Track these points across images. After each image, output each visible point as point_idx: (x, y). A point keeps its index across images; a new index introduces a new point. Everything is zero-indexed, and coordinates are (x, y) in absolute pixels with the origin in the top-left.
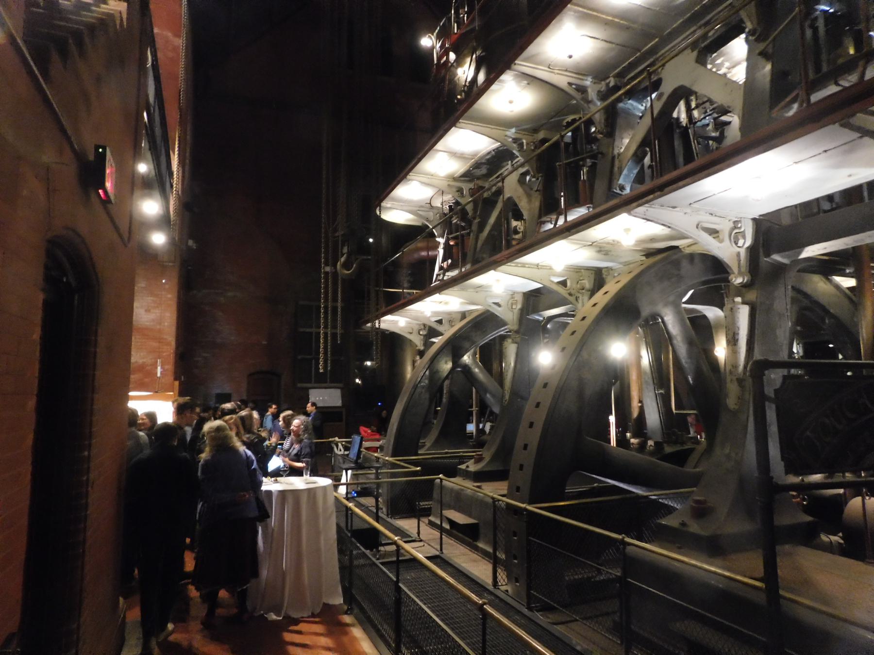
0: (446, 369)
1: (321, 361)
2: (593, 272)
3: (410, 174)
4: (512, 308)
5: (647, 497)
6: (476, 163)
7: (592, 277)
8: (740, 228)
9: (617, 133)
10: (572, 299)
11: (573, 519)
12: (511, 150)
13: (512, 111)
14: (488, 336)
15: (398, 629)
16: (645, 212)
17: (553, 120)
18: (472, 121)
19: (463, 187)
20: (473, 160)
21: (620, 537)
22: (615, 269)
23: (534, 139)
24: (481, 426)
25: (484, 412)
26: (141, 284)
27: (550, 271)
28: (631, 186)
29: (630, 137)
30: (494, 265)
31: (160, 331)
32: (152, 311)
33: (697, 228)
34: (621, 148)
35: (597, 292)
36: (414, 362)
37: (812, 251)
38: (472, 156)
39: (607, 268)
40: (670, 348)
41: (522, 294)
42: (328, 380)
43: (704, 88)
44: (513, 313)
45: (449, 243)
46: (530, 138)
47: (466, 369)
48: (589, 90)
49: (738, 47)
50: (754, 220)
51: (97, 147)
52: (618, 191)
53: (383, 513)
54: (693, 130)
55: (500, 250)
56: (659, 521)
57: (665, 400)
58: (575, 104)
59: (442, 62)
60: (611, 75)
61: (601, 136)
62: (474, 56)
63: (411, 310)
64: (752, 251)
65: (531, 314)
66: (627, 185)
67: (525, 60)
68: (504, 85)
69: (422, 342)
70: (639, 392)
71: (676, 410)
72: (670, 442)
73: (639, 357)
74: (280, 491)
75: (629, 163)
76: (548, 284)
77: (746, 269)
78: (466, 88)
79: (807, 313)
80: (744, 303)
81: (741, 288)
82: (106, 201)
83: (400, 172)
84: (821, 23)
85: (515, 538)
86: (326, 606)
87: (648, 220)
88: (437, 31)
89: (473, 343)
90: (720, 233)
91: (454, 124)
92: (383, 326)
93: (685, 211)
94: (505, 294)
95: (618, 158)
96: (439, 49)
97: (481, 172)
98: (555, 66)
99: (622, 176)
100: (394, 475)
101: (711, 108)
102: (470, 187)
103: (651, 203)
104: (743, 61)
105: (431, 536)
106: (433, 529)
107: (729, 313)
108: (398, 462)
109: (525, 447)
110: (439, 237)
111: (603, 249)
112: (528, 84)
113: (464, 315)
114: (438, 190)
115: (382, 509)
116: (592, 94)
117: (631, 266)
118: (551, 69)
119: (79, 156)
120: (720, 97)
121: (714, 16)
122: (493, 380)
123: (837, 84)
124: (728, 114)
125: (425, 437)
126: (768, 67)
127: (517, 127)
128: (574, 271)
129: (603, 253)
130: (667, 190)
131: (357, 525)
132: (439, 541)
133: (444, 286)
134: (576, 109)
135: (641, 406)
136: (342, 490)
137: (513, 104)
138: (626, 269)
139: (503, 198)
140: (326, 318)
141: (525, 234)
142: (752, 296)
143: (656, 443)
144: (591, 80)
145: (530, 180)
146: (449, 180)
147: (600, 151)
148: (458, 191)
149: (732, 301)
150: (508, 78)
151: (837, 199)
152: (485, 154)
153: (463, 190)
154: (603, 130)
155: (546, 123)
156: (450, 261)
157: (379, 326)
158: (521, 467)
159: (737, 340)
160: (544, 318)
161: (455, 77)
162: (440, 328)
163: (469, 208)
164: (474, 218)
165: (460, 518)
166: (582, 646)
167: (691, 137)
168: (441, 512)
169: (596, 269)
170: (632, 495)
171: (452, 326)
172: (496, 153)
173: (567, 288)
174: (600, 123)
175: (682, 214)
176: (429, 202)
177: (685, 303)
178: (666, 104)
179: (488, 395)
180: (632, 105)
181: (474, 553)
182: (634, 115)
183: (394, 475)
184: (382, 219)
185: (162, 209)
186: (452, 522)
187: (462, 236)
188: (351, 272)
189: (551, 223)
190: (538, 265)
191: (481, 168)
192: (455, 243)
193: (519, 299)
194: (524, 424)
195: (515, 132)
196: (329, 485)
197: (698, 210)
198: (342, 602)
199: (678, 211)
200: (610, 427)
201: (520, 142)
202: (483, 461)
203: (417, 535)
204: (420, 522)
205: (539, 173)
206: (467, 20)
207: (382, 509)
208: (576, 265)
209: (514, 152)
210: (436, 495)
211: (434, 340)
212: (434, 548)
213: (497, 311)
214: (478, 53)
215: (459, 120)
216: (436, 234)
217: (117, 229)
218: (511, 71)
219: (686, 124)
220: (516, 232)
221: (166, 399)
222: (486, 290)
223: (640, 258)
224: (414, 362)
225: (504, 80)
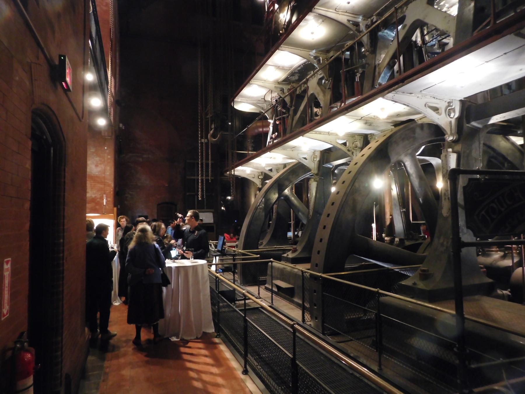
1: (200, 193)
2: (363, 137)
4: (314, 160)
5: (393, 270)
6: (292, 72)
7: (362, 139)
8: (452, 106)
9: (378, 51)
11: (349, 281)
13: (313, 39)
15: (246, 345)
16: (393, 97)
18: (288, 46)
19: (284, 88)
20: (290, 71)
21: (376, 290)
23: (327, 57)
24: (296, 233)
25: (298, 225)
26: (91, 150)
27: (337, 136)
29: (385, 53)
30: (302, 133)
31: (104, 178)
32: (99, 166)
33: (425, 106)
34: (380, 60)
37: (496, 119)
39: (371, 134)
40: (410, 183)
42: (205, 207)
43: (433, 20)
44: (315, 163)
46: (325, 56)
47: (287, 198)
48: (361, 24)
50: (461, 101)
51: (60, 56)
53: (238, 283)
54: (425, 48)
55: (306, 124)
56: (400, 283)
57: (406, 215)
61: (368, 53)
64: (459, 120)
67: (320, 6)
69: (260, 183)
70: (390, 209)
71: (413, 220)
72: (408, 239)
73: (390, 189)
74: (176, 267)
75: (385, 69)
79: (493, 160)
81: (451, 143)
82: (67, 90)
83: (246, 78)
85: (315, 294)
86: (205, 334)
87: (396, 102)
90: (439, 109)
91: (277, 48)
92: (237, 173)
93: (418, 96)
97: (296, 78)
98: (339, 9)
99: (380, 78)
100: (243, 259)
101: (437, 33)
102: (289, 88)
103: (397, 91)
105: (266, 296)
106: (268, 292)
108: (247, 253)
109: (321, 240)
110: (270, 119)
111: (368, 122)
112: (323, 21)
113: (285, 165)
115: (237, 281)
116: (362, 27)
117: (385, 132)
118: (337, 11)
119: (49, 61)
120: (441, 26)
122: (302, 204)
124: (447, 38)
125: (263, 239)
127: (316, 49)
128: (351, 136)
129: (367, 124)
130: (406, 82)
131: (222, 288)
132: (271, 298)
134: (352, 37)
135: (391, 218)
136: (213, 268)
137: (313, 34)
138: (383, 134)
140: (202, 170)
141: (321, 116)
142: (458, 147)
143: (400, 240)
144: (362, 18)
145: (325, 83)
149: (445, 151)
150: (310, 18)
152: (297, 67)
153: (284, 90)
154: (369, 49)
155: (334, 46)
156: (276, 134)
157: (234, 173)
158: (319, 252)
162: (271, 174)
163: (287, 100)
164: (291, 107)
165: (283, 285)
166: (354, 354)
167: (424, 53)
168: (272, 281)
170: (386, 268)
171: (278, 172)
172: (304, 66)
173: (347, 147)
174: (367, 44)
175: (416, 98)
177: (417, 155)
179: (300, 214)
180: (387, 33)
181: (292, 304)
183: (243, 259)
184: (235, 109)
185: (103, 103)
186: (278, 287)
187: (284, 118)
188: (216, 140)
190: (329, 133)
191: (295, 75)
193: (318, 154)
194: (320, 227)
195: (315, 53)
196: (205, 264)
198: (214, 331)
199: (413, 96)
200: (372, 232)
201: (318, 59)
202: (297, 251)
203: (258, 295)
204: (260, 288)
207: (237, 281)
209: (315, 65)
210: (269, 272)
211: (267, 181)
212: (268, 302)
213: (305, 162)
216: (268, 118)
217: (74, 109)
218: (312, 13)
219: (421, 45)
220: (316, 115)
221: (110, 218)
223: (390, 127)
224: (256, 195)
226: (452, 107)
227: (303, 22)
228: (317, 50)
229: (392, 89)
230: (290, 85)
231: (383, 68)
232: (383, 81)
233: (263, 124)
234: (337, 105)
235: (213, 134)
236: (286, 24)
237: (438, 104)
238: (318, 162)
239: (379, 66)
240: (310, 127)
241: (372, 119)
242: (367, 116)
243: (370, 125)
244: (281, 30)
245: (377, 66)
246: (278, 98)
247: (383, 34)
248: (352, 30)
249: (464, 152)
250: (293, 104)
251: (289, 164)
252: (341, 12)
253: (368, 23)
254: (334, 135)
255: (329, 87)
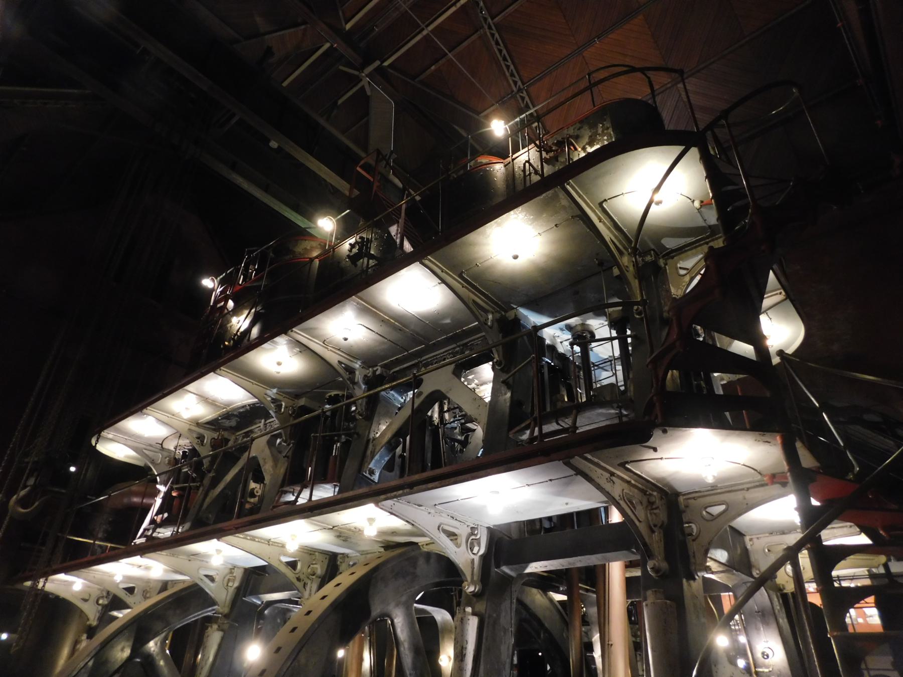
0: (119, 659)
2: (328, 557)
3: (148, 408)
4: (227, 585)
6: (227, 413)
7: (326, 562)
8: (476, 535)
9: (376, 419)
10: (299, 585)
12: (268, 409)
13: (279, 373)
14: (189, 617)
17: (315, 390)
18: (235, 372)
19: (205, 435)
20: (224, 410)
22: (351, 557)
23: (294, 404)
27: (282, 549)
28: (381, 472)
30: (219, 534)
33: (439, 529)
34: (377, 433)
35: (327, 584)
36: (76, 642)
37: (535, 567)
38: (225, 405)
39: (343, 554)
41: (243, 570)
43: (457, 398)
45: (171, 493)
46: (291, 403)
47: (149, 659)
48: (357, 373)
49: (486, 371)
50: (488, 528)
52: (367, 475)
55: (230, 519)
58: (341, 381)
59: (218, 306)
60: (380, 364)
61: (360, 417)
62: (253, 310)
63: (98, 571)
64: (485, 558)
65: (248, 596)
66: (377, 471)
68: (277, 347)
69: (98, 615)
76: (275, 564)
77: (478, 579)
78: (236, 337)
80: (474, 614)
81: (471, 597)
84: (546, 370)
88: (221, 277)
89: (168, 624)
91: (214, 370)
93: (429, 511)
94: (223, 566)
95: (372, 442)
96: (219, 294)
97: (231, 423)
98: (330, 343)
99: (373, 461)
104: (490, 382)
107: (458, 623)
110: (161, 484)
113: (165, 585)
114: (175, 431)
116: (359, 377)
117: (369, 556)
120: (468, 409)
121: (470, 341)
123: (558, 424)
126: (509, 395)
128: (308, 553)
129: (341, 538)
130: (415, 488)
133: (153, 546)
134: (341, 386)
138: (362, 559)
139: (249, 454)
142: (481, 607)
145: (280, 443)
146: (190, 423)
147: (357, 431)
148: (198, 438)
149: (462, 611)
151: (555, 520)
156: (166, 515)
157: (44, 586)
159: (465, 655)
160: (262, 602)
161: (228, 323)
162: (128, 599)
164: (209, 472)
169: (331, 554)
172: (251, 408)
173: (297, 571)
176: (161, 443)
178: (423, 403)
180: (393, 396)
182: (394, 405)
187: (190, 488)
188: (27, 512)
189: (293, 495)
190: (269, 541)
192: (178, 495)
193: (238, 574)
195: (277, 393)
197: (441, 512)
199: (422, 510)
201: (279, 403)
205: (291, 439)
206: (254, 276)
208: (310, 546)
209: (271, 412)
211: (115, 613)
213: (210, 588)
214: (259, 308)
215: (221, 367)
219: (438, 424)
220: (252, 495)
222: (201, 559)
223: (378, 549)
224: (76, 642)
225: (277, 342)
226: (476, 536)
227: (268, 344)
228: (280, 390)
229: (393, 494)
230: (218, 433)
231: (381, 446)
232: (376, 467)
233: (146, 488)
234: (294, 489)
235: (25, 496)
236: (239, 334)
237: (458, 528)
238: (236, 590)
239: (374, 442)
240: (236, 526)
241: (351, 532)
242: (341, 526)
243: (345, 540)
244: (227, 340)
245: (371, 441)
246: (188, 449)
247: (388, 395)
248: (342, 377)
249: (490, 616)
250: (214, 468)
251: (174, 582)
252: (332, 347)
253: (369, 373)
254: (278, 546)
255: (287, 454)
